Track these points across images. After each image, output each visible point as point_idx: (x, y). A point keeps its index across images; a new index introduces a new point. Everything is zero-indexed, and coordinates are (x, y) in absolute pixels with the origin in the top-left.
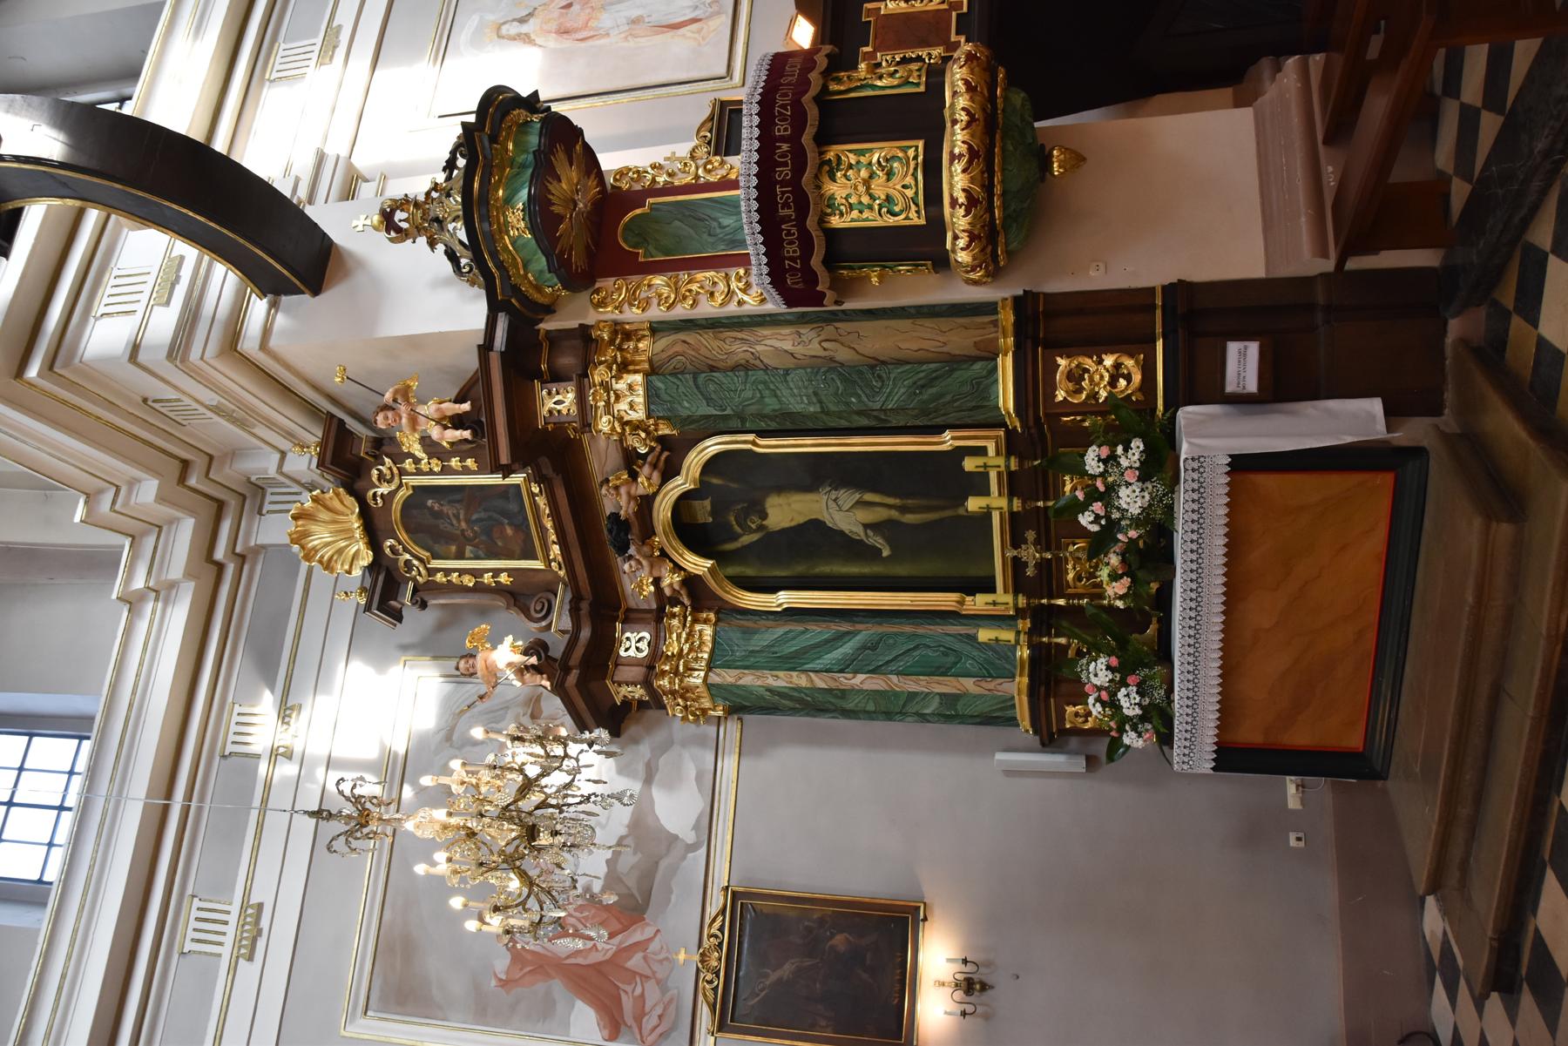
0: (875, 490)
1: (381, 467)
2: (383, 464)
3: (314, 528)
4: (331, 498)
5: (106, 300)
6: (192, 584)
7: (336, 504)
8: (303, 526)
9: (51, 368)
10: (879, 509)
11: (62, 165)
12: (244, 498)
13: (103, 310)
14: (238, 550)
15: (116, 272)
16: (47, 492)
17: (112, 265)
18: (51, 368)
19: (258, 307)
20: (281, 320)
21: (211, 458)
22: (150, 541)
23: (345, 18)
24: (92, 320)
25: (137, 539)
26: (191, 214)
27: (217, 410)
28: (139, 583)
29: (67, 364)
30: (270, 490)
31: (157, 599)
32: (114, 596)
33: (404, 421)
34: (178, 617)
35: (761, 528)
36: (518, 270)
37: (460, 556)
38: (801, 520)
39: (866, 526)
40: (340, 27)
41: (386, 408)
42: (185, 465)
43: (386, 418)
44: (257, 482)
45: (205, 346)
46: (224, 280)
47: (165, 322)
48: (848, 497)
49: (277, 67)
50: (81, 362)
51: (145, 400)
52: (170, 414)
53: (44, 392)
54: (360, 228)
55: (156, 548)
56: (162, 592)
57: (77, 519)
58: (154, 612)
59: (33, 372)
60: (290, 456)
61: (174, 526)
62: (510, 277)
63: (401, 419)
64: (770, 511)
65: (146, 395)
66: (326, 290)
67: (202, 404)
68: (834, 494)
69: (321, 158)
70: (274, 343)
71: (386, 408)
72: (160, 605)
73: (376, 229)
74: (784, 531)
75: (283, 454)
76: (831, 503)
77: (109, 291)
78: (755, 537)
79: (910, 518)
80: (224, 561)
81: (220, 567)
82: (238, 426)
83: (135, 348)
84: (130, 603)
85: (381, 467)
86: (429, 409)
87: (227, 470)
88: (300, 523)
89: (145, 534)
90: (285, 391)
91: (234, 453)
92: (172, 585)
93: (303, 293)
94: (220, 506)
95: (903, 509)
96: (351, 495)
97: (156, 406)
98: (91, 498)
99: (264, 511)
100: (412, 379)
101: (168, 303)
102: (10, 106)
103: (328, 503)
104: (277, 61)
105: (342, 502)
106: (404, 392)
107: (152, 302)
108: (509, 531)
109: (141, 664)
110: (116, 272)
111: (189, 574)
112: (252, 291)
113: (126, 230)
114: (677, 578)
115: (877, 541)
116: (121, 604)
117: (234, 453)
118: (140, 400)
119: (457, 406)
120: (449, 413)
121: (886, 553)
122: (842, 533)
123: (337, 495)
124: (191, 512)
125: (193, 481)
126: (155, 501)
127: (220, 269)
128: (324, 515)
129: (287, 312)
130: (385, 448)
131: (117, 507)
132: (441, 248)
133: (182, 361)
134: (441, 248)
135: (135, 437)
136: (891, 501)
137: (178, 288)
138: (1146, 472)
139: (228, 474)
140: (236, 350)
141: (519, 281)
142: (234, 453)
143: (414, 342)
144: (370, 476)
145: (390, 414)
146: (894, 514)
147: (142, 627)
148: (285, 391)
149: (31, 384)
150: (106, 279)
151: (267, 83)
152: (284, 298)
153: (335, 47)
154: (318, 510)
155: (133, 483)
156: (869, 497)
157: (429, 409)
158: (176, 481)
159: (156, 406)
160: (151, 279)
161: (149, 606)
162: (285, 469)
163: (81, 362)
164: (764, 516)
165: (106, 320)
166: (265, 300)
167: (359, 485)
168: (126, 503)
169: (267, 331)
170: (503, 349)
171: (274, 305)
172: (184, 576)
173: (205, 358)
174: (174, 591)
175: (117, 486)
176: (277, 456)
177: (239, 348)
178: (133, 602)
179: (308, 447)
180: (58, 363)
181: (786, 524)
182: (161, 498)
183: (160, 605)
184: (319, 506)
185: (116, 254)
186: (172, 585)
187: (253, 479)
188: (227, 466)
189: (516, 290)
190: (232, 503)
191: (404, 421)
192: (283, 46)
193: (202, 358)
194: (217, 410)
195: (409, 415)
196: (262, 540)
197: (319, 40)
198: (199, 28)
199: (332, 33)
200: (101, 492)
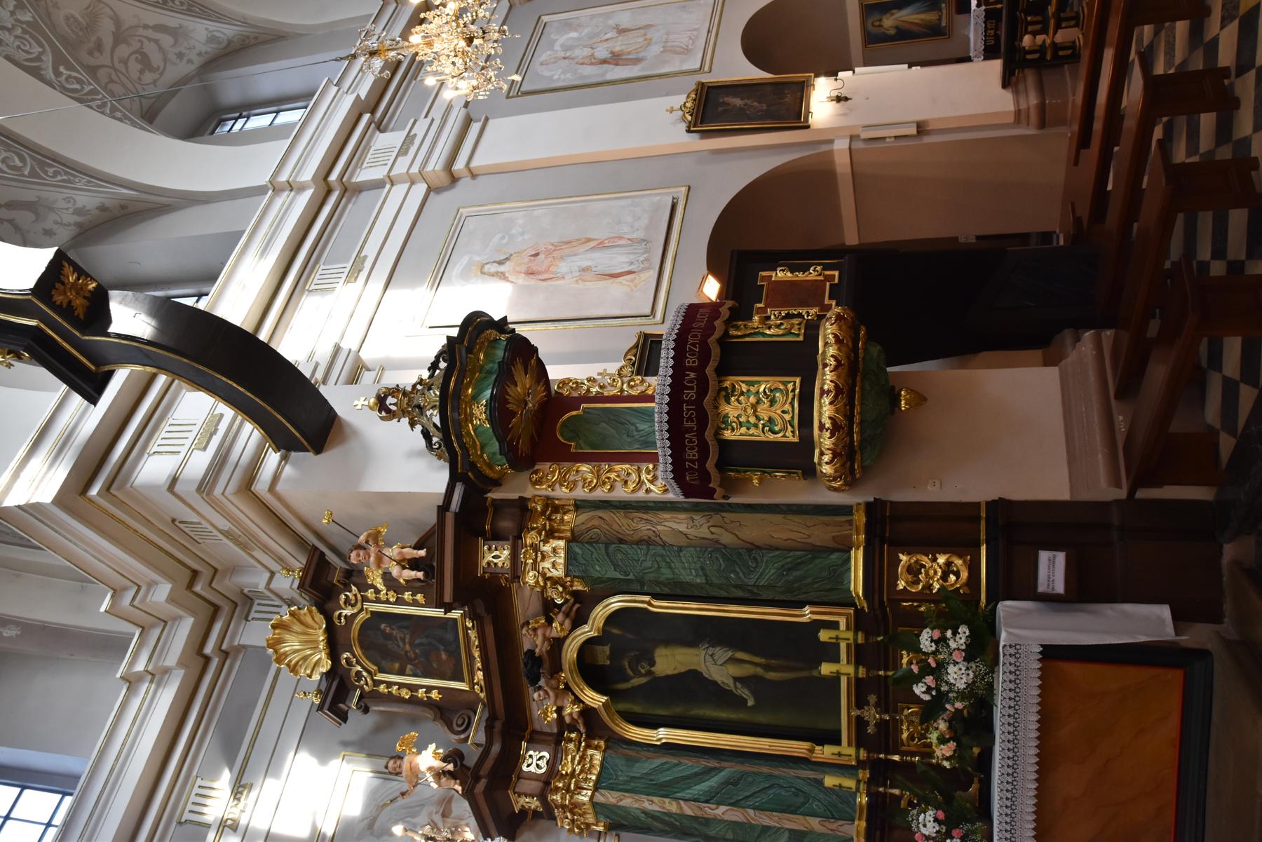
0: (744, 650)
1: (348, 593)
2: (350, 591)
3: (287, 637)
4: (305, 614)
5: (160, 442)
6: (182, 671)
7: (309, 620)
8: (279, 634)
9: (108, 489)
10: (748, 666)
11: (149, 343)
12: (236, 605)
13: (156, 449)
14: (224, 647)
15: (171, 421)
16: (84, 584)
17: (169, 416)
18: (108, 489)
19: (273, 458)
20: (288, 470)
21: (216, 570)
22: (156, 632)
23: (370, 251)
24: (146, 455)
25: (146, 630)
26: (235, 385)
27: (227, 534)
28: (140, 667)
29: (121, 488)
30: (257, 601)
31: (151, 682)
32: (118, 675)
33: (372, 559)
34: (166, 698)
35: (649, 673)
36: (476, 451)
37: (401, 672)
38: (683, 669)
39: (736, 679)
40: (366, 257)
41: (360, 547)
42: (195, 574)
43: (358, 555)
44: (249, 594)
45: (227, 484)
46: (250, 434)
47: (200, 462)
48: (722, 654)
49: (316, 281)
50: (131, 486)
51: (173, 521)
52: (192, 534)
53: (100, 507)
54: (359, 407)
55: (159, 639)
56: (157, 676)
57: (102, 609)
58: (147, 692)
59: (94, 491)
60: (277, 575)
61: (177, 623)
62: (469, 456)
63: (369, 557)
64: (658, 660)
65: (175, 517)
66: (327, 450)
67: (212, 525)
68: (711, 651)
69: (337, 350)
70: (280, 487)
71: (360, 547)
72: (293, 193)
73: (371, 408)
74: (668, 678)
75: (273, 574)
76: (708, 657)
77: (163, 435)
78: (643, 680)
79: (772, 675)
80: (211, 655)
81: (207, 660)
82: (241, 548)
83: (174, 480)
84: (130, 682)
85: (348, 593)
86: (393, 552)
87: (227, 581)
88: (277, 631)
89: (153, 626)
90: (282, 525)
91: (234, 569)
92: (167, 671)
93: (308, 451)
94: (216, 609)
95: (767, 668)
96: (321, 613)
97: (181, 526)
98: (117, 593)
99: (250, 618)
100: (382, 527)
101: (205, 449)
102: (123, 299)
103: (302, 618)
104: (316, 278)
105: (313, 619)
106: (375, 537)
107: (193, 447)
108: (444, 656)
109: (128, 735)
110: (171, 421)
111: (181, 663)
112: (270, 446)
113: (184, 391)
114: (576, 709)
115: (744, 692)
116: (122, 682)
117: (234, 569)
118: (170, 520)
119: (415, 551)
120: (408, 557)
121: (750, 703)
122: (715, 683)
123: (310, 611)
124: (192, 612)
125: (198, 588)
126: (166, 601)
127: (248, 427)
128: (297, 627)
129: (294, 465)
130: (354, 579)
131: (136, 603)
132: (419, 428)
133: (208, 494)
134: (419, 428)
135: (161, 549)
136: (757, 660)
137: (214, 438)
138: (971, 653)
139: (226, 585)
140: (250, 490)
141: (476, 459)
142: (234, 569)
143: (388, 498)
144: (338, 599)
145: (362, 553)
146: (759, 671)
147: (135, 703)
148: (282, 525)
149: (90, 500)
150: (162, 426)
151: (307, 292)
152: (293, 454)
153: (360, 271)
154: (293, 623)
155: (152, 584)
156: (740, 655)
157: (393, 552)
158: (185, 586)
159: (181, 526)
160: (195, 429)
161: (144, 687)
162: (272, 586)
163: (131, 486)
164: (653, 663)
165: (156, 457)
166: (279, 454)
167: (329, 606)
168: (144, 600)
169: (276, 477)
170: (457, 511)
171: (284, 458)
172: (177, 664)
173: (226, 494)
174: (167, 676)
175: (139, 586)
176: (268, 575)
177: (252, 488)
178: (132, 682)
179: (293, 571)
180: (114, 486)
181: (670, 672)
182: (171, 599)
183: (153, 686)
184: (295, 620)
185: (175, 406)
186: (167, 671)
187: (246, 591)
188: (227, 579)
189: (473, 466)
190: (226, 608)
191: (372, 559)
192: (322, 267)
193: (223, 494)
194: (227, 534)
195: (377, 555)
196: (245, 641)
197: (349, 265)
198: (264, 251)
199: (359, 261)
200: (125, 589)
